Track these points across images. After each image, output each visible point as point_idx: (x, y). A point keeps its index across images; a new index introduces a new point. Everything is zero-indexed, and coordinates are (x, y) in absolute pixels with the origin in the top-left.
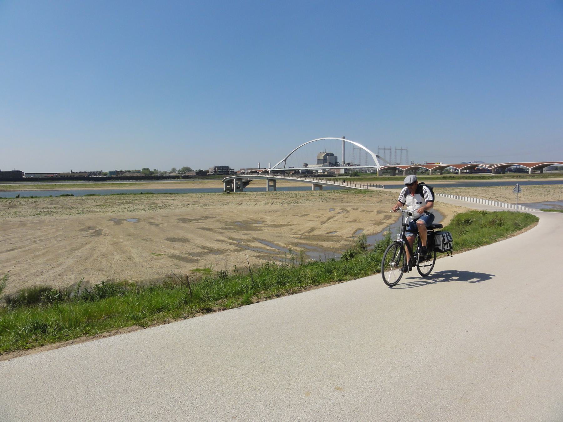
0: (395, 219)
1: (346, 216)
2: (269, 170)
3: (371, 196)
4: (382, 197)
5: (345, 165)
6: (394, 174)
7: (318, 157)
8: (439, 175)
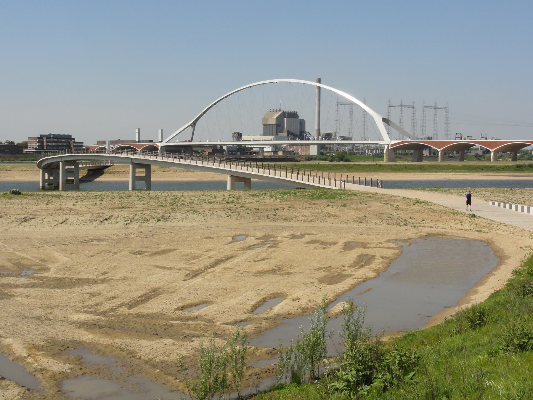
0: (381, 266)
1: (263, 255)
2: (159, 144)
3: (345, 206)
4: (369, 207)
5: (320, 137)
6: (420, 158)
7: (265, 119)
8: (510, 163)
